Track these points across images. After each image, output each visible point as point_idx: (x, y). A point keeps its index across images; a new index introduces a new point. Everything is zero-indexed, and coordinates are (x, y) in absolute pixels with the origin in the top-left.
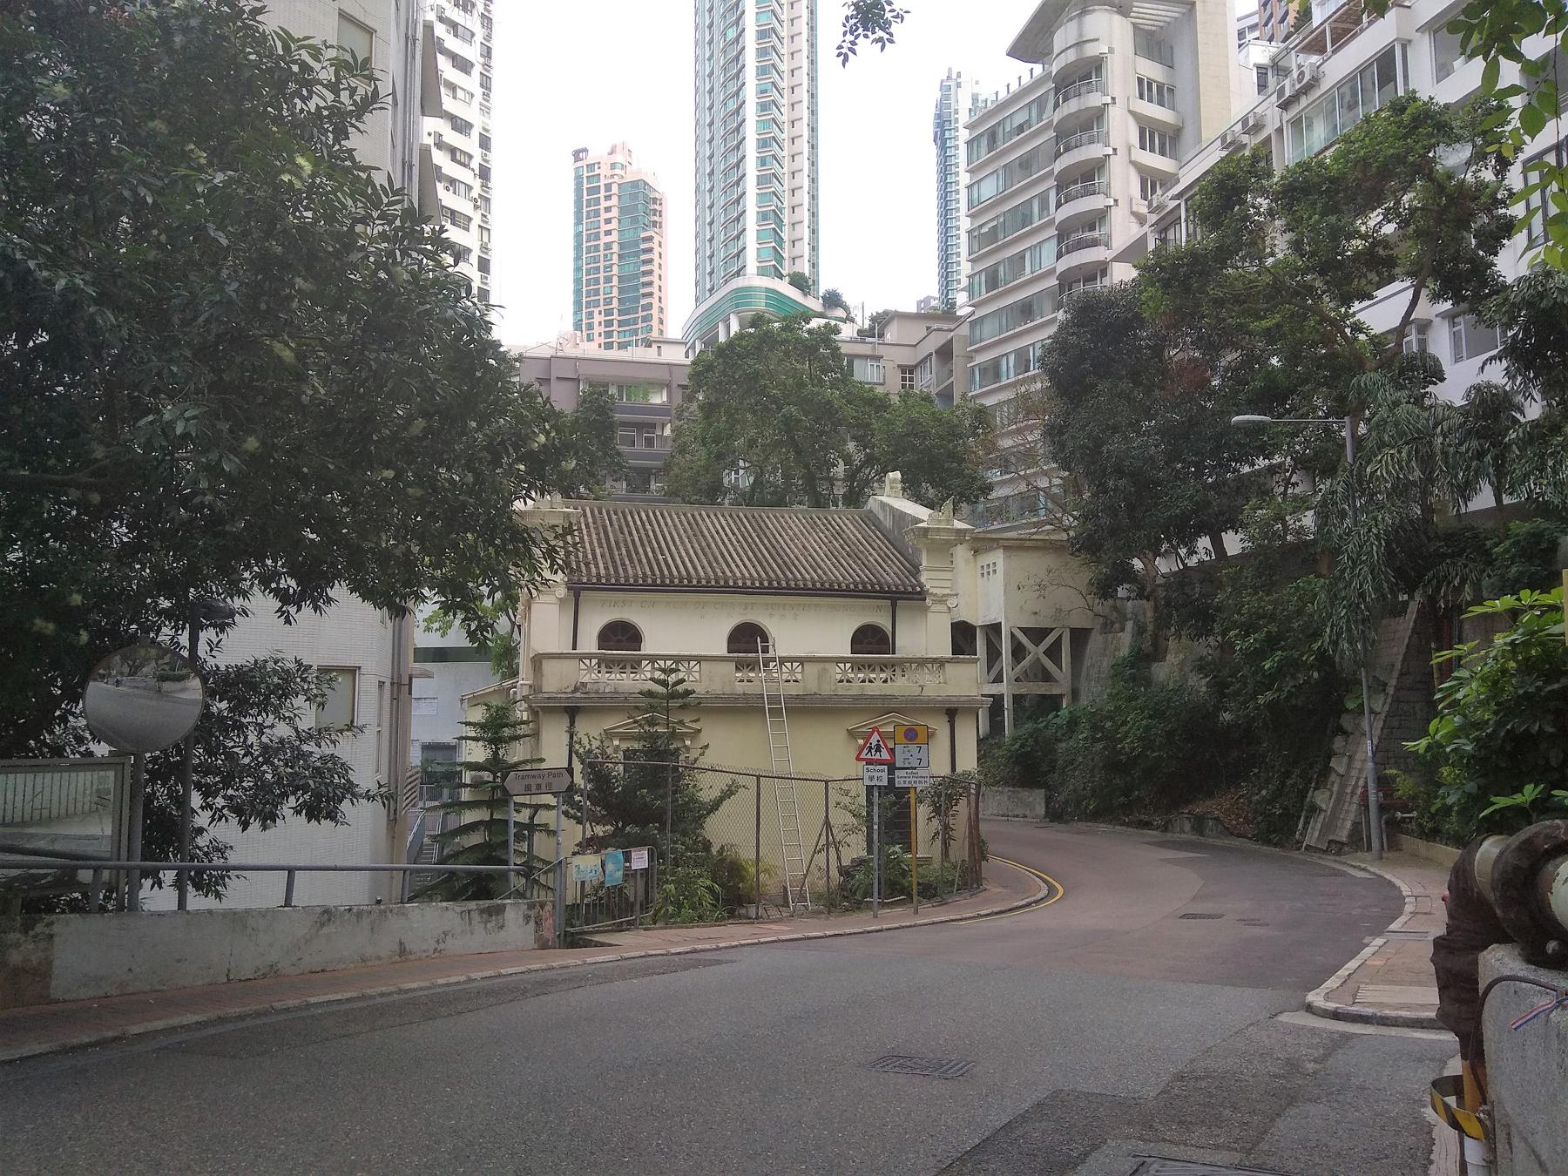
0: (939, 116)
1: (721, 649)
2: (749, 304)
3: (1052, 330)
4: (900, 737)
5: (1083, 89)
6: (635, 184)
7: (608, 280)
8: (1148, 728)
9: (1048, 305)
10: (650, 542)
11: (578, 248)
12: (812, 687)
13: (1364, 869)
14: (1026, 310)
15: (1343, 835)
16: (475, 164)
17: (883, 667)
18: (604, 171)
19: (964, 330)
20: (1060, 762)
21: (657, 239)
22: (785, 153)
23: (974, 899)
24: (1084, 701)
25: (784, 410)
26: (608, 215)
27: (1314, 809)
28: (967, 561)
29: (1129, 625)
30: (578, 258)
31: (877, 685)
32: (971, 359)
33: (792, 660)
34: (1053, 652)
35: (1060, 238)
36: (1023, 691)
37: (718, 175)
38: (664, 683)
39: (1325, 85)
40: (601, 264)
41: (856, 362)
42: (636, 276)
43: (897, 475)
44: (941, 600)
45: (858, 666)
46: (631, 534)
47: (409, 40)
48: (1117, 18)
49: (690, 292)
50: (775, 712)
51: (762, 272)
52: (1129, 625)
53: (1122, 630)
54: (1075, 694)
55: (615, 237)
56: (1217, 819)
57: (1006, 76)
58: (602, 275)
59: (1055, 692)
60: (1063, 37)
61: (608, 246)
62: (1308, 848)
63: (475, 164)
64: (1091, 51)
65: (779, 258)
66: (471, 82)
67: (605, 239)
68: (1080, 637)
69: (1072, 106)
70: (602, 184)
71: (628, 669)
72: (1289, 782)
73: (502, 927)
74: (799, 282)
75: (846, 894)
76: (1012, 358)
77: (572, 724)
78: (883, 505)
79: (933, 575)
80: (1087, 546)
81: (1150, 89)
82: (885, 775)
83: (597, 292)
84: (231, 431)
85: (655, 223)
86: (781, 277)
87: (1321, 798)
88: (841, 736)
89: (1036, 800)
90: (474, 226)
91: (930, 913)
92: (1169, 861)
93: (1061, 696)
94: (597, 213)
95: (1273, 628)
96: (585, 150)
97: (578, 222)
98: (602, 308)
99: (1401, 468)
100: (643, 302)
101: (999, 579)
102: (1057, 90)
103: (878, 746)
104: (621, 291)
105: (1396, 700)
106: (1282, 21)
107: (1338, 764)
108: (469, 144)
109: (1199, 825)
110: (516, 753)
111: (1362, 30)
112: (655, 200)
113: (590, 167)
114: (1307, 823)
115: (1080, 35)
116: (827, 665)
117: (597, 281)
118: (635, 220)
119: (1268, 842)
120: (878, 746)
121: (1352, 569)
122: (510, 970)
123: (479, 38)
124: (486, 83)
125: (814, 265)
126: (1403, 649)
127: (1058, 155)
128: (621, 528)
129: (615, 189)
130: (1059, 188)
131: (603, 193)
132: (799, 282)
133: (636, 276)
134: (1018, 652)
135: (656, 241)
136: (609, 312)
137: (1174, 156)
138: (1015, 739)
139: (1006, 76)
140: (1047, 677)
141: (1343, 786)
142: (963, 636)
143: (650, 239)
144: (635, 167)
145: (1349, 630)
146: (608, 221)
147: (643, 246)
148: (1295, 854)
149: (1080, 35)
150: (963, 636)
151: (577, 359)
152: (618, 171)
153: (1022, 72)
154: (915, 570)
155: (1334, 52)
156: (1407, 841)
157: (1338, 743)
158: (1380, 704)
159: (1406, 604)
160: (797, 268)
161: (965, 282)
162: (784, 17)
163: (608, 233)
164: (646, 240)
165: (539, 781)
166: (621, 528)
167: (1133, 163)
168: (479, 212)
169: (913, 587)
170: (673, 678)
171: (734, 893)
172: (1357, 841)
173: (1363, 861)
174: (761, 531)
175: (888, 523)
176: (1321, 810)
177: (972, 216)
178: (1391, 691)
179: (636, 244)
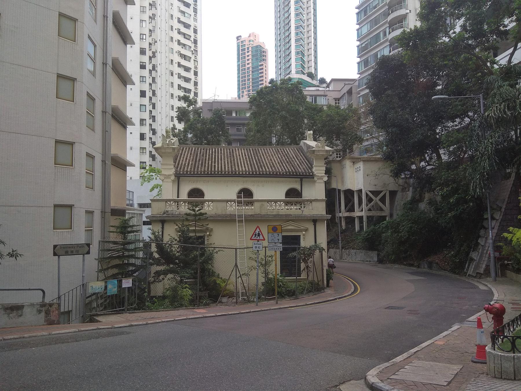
3: (372, 71)
6: (257, 47)
7: (249, 80)
8: (411, 227)
11: (239, 70)
12: (258, 211)
13: (486, 286)
15: (482, 271)
16: (192, 39)
18: (247, 43)
20: (383, 241)
21: (264, 65)
22: (305, 30)
23: (315, 296)
24: (395, 217)
26: (248, 58)
27: (472, 260)
28: (350, 167)
29: (411, 189)
30: (238, 73)
31: (294, 210)
32: (359, 94)
35: (390, 45)
36: (371, 214)
37: (282, 40)
38: (194, 210)
40: (246, 75)
41: (318, 98)
42: (258, 78)
43: (312, 132)
45: (287, 203)
50: (240, 221)
51: (297, 72)
52: (411, 189)
53: (409, 191)
54: (391, 215)
55: (250, 65)
56: (437, 263)
59: (383, 215)
61: (248, 68)
62: (469, 275)
63: (192, 39)
65: (303, 67)
66: (190, 11)
68: (393, 194)
72: (462, 248)
73: (21, 316)
74: (310, 75)
75: (272, 291)
78: (305, 143)
79: (317, 168)
80: (388, 158)
83: (245, 84)
84: (458, 194)
85: (264, 59)
86: (304, 74)
87: (474, 255)
89: (374, 255)
91: (286, 303)
92: (408, 281)
95: (455, 185)
96: (240, 36)
98: (247, 89)
101: (361, 172)
103: (259, 234)
104: (253, 83)
105: (505, 214)
107: (481, 241)
108: (190, 32)
109: (430, 267)
110: (131, 237)
112: (264, 52)
113: (242, 42)
114: (469, 265)
116: (263, 203)
117: (245, 81)
118: (257, 59)
119: (455, 273)
120: (259, 234)
121: (481, 158)
122: (9, 337)
124: (195, 10)
125: (316, 69)
126: (509, 193)
127: (389, 14)
128: (203, 155)
129: (250, 49)
130: (390, 27)
132: (310, 75)
133: (258, 78)
134: (370, 200)
135: (264, 65)
136: (249, 91)
138: (366, 232)
140: (381, 210)
141: (483, 250)
143: (262, 65)
144: (257, 41)
146: (248, 60)
147: (260, 68)
148: (463, 278)
152: (251, 43)
154: (311, 168)
156: (508, 273)
157: (482, 232)
158: (498, 216)
159: (510, 174)
160: (310, 71)
163: (248, 64)
165: (73, 249)
166: (203, 155)
169: (309, 173)
172: (487, 273)
173: (487, 282)
175: (305, 149)
176: (475, 260)
178: (503, 210)
179: (258, 67)
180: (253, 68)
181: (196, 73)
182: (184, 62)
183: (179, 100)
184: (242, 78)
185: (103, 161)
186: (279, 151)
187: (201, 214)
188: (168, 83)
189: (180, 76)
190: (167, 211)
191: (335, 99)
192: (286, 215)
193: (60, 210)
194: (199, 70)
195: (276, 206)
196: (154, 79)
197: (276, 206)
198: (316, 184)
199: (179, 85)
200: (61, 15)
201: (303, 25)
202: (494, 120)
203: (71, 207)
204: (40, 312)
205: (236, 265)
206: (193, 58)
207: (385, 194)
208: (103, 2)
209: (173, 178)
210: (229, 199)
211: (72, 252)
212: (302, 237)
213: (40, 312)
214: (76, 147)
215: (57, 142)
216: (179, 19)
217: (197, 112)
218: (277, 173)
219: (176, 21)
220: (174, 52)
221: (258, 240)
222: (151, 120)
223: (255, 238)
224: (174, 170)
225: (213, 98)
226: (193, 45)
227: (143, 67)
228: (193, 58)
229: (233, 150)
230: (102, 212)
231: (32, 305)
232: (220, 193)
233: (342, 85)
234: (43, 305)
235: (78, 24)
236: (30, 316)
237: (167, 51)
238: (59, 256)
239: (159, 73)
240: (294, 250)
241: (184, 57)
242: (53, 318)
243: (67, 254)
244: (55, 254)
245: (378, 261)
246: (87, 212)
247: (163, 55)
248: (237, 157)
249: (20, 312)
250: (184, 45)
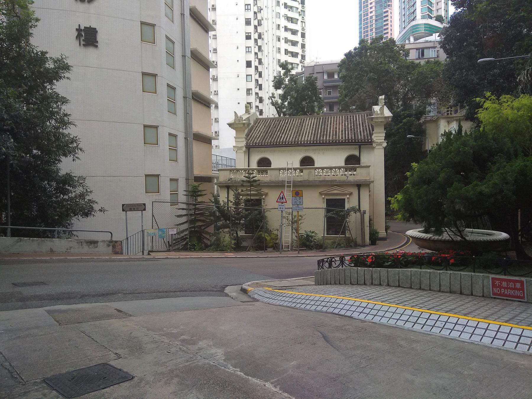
1: (342, 164)
2: (416, 31)
7: (371, 30)
30: (360, 24)
41: (425, 50)
42: (382, 27)
51: (423, 17)
55: (374, 13)
58: (369, 29)
61: (371, 17)
65: (430, 11)
71: (261, 173)
85: (389, 5)
86: (431, 18)
88: (318, 194)
90: (299, 22)
94: (367, 6)
97: (360, 10)
118: (381, 6)
133: (382, 27)
154: (371, 135)
160: (439, 14)
163: (371, 12)
164: (385, 12)
168: (301, 16)
171: (276, 247)
180: (376, 16)
181: (303, 35)
182: (291, 26)
184: (364, 29)
185: (185, 138)
186: (348, 119)
187: (255, 181)
188: (275, 49)
189: (286, 41)
190: (231, 179)
192: (331, 181)
193: (149, 178)
195: (323, 172)
196: (260, 48)
197: (323, 172)
199: (286, 50)
200: (142, 23)
203: (158, 176)
204: (109, 246)
205: (153, 215)
208: (180, 2)
209: (244, 149)
210: (281, 167)
211: (134, 209)
212: (346, 200)
213: (109, 246)
214: (160, 129)
215: (145, 126)
217: (293, 79)
218: (336, 141)
220: (281, 16)
221: (282, 203)
222: (258, 88)
224: (245, 142)
226: (301, 5)
227: (248, 37)
228: (300, 19)
230: (186, 179)
231: (104, 241)
232: (286, 162)
234: (111, 241)
235: (156, 28)
236: (102, 248)
237: (274, 16)
238: (126, 212)
239: (266, 41)
240: (342, 211)
241: (291, 20)
242: (117, 250)
243: (131, 210)
244: (123, 210)
246: (171, 180)
247: (270, 10)
249: (96, 245)
250: (291, 7)
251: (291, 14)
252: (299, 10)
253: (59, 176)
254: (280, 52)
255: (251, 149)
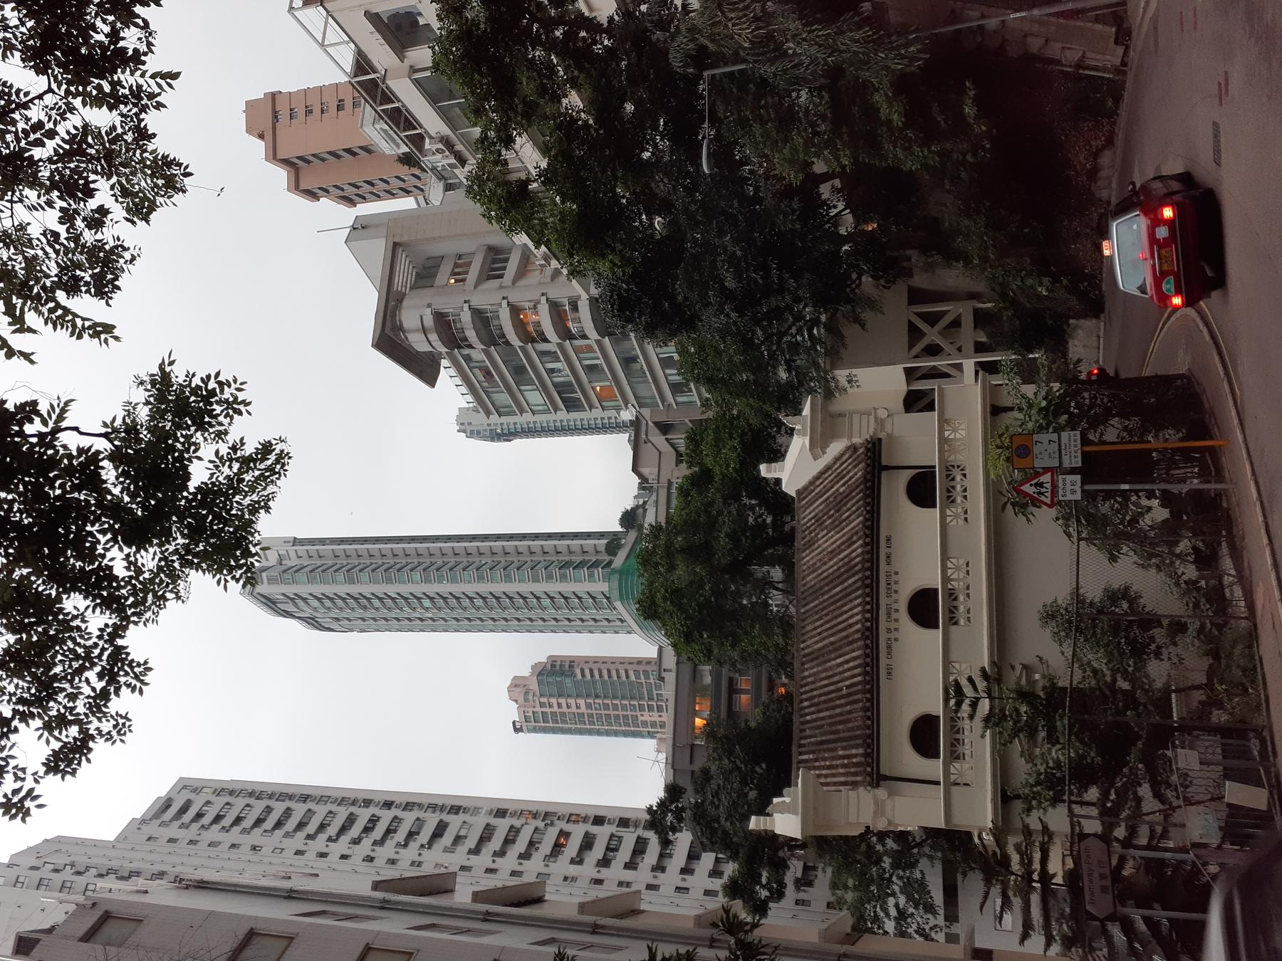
0: (492, 440)
4: (1023, 463)
5: (459, 326)
9: (625, 344)
10: (831, 700)
14: (628, 361)
16: (517, 823)
17: (950, 477)
19: (646, 412)
22: (515, 559)
25: (711, 565)
33: (944, 569)
34: (932, 319)
39: (446, 131)
44: (880, 423)
46: (823, 718)
47: (385, 906)
48: (405, 303)
49: (622, 637)
55: (581, 702)
57: (450, 392)
60: (419, 343)
61: (589, 706)
64: (429, 321)
66: (455, 821)
67: (583, 709)
69: (471, 334)
70: (538, 709)
76: (668, 371)
77: (887, 468)
81: (459, 274)
82: (1070, 478)
90: (568, 827)
93: (976, 311)
94: (563, 714)
98: (638, 713)
99: (745, 15)
100: (633, 678)
102: (459, 347)
103: (1037, 485)
106: (419, 178)
108: (502, 825)
111: (404, 106)
112: (553, 666)
115: (417, 331)
120: (1037, 485)
123: (421, 815)
124: (455, 810)
125: (602, 535)
127: (508, 343)
129: (544, 700)
131: (547, 710)
134: (933, 350)
136: (641, 708)
137: (509, 251)
139: (450, 392)
140: (956, 323)
142: (916, 402)
145: (898, 48)
149: (417, 331)
150: (916, 402)
151: (674, 744)
153: (447, 376)
155: (421, 127)
160: (602, 548)
161: (613, 413)
162: (404, 562)
165: (1096, 875)
167: (514, 282)
168: (557, 822)
170: (968, 691)
174: (817, 592)
177: (556, 409)
181: (599, 821)
183: (663, 869)
191: (679, 462)
194: (592, 813)
198: (897, 433)
201: (503, 564)
202: (760, 28)
206: (562, 825)
207: (916, 314)
209: (881, 793)
216: (470, 852)
219: (474, 860)
220: (545, 870)
223: (1048, 495)
225: (663, 766)
228: (562, 825)
229: (805, 656)
233: (646, 449)
241: (558, 848)
245: (1097, 317)
248: (824, 639)
250: (531, 844)
251: (546, 847)
252: (541, 825)
253: (1159, 690)
254: (574, 879)
255: (885, 770)
